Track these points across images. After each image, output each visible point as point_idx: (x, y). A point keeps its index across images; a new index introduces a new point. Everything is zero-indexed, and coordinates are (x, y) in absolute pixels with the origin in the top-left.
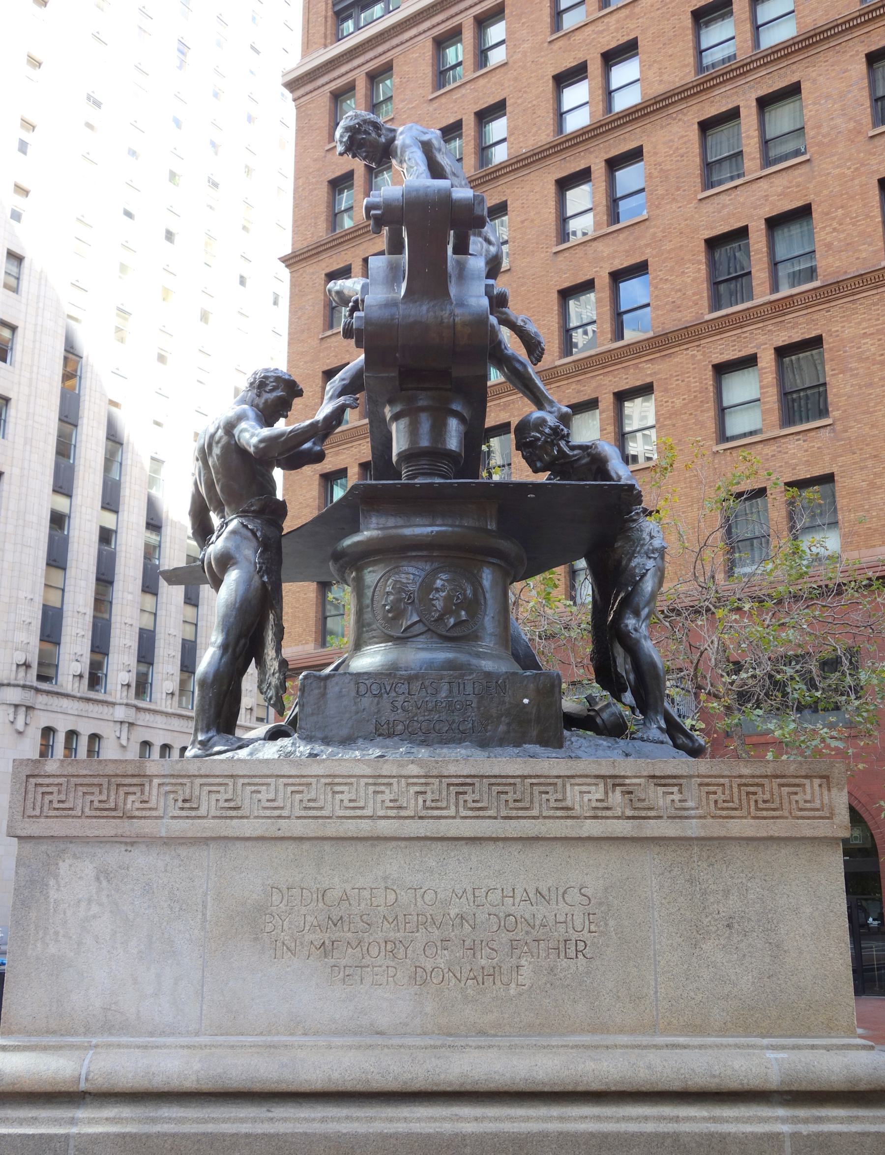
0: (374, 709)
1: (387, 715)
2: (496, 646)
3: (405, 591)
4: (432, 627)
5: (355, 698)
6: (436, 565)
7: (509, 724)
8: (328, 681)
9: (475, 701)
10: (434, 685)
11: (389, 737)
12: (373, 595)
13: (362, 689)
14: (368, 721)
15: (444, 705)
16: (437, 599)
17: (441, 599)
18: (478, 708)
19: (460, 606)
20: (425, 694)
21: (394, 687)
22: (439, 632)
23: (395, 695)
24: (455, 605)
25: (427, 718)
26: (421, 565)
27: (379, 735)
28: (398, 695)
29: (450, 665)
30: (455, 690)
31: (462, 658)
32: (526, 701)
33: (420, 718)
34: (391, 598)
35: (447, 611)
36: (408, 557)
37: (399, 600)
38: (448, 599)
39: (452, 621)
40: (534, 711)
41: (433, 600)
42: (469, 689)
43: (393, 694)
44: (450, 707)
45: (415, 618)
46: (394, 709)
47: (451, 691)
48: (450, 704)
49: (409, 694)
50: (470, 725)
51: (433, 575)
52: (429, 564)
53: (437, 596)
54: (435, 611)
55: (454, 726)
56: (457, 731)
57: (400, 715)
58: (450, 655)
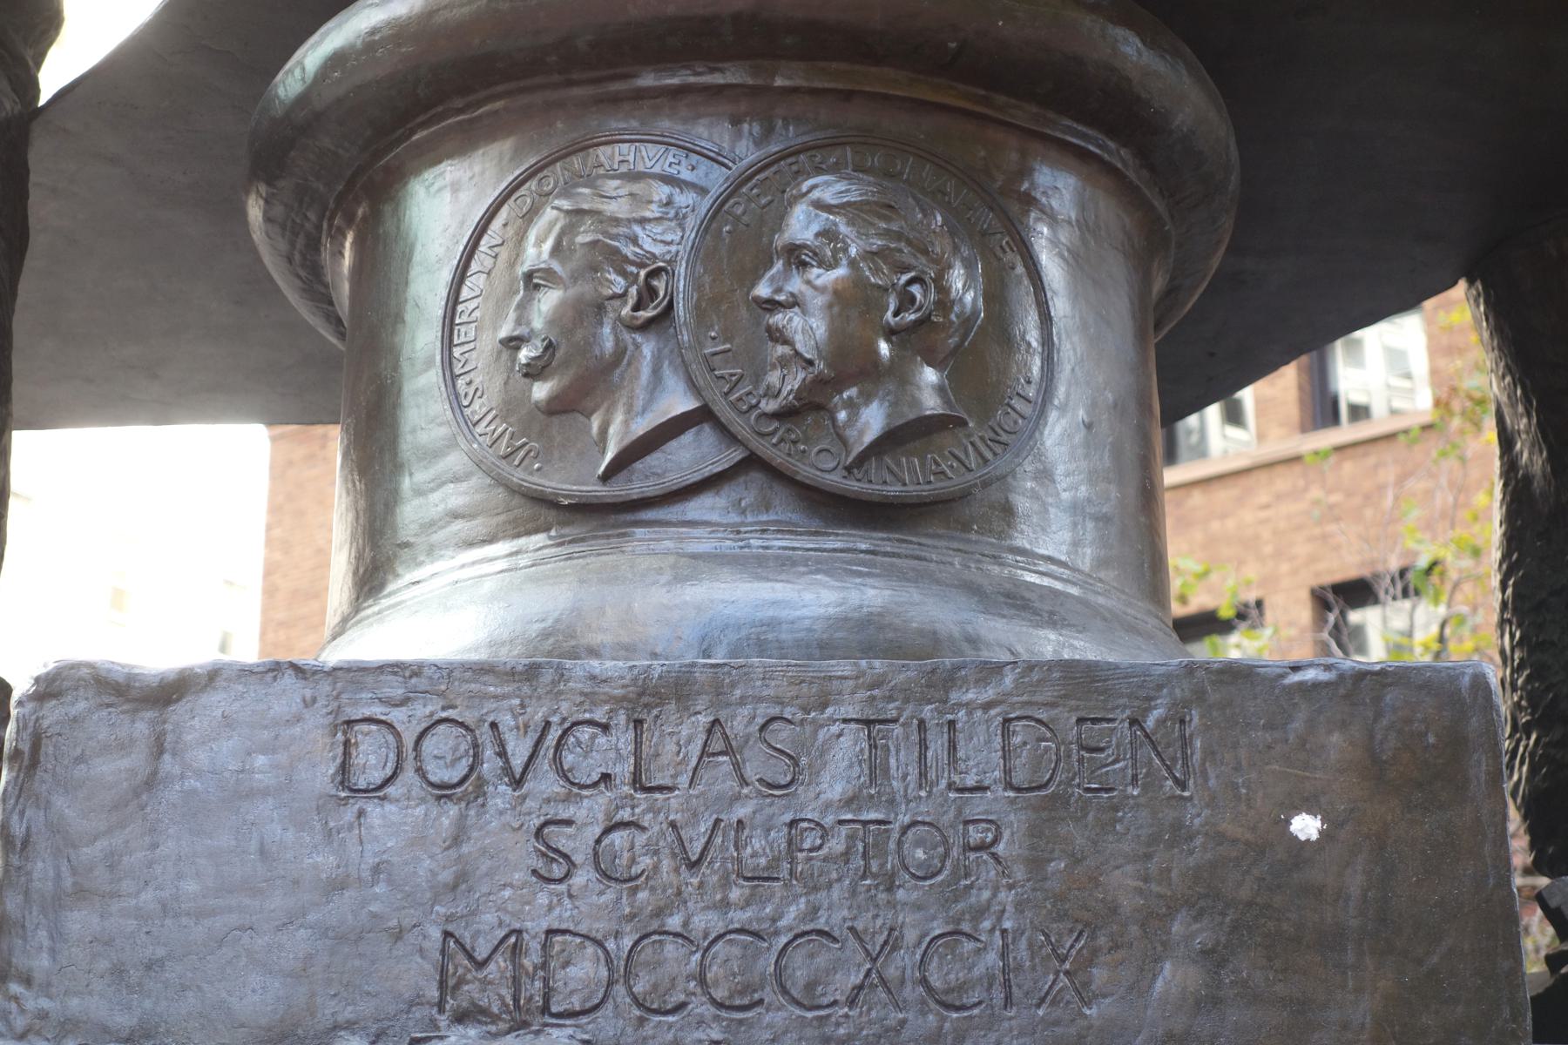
0: (429, 867)
1: (512, 900)
2: (1108, 575)
3: (618, 261)
4: (765, 449)
5: (328, 803)
6: (788, 136)
7: (1213, 958)
8: (178, 711)
9: (1015, 823)
10: (782, 736)
11: (520, 1026)
12: (454, 299)
13: (372, 759)
14: (398, 935)
15: (836, 845)
16: (795, 302)
17: (817, 301)
18: (1036, 864)
19: (918, 338)
20: (732, 784)
21: (553, 741)
22: (805, 472)
23: (556, 787)
24: (890, 333)
25: (739, 917)
26: (711, 133)
27: (461, 1018)
28: (575, 787)
29: (868, 637)
30: (901, 761)
31: (933, 611)
32: (1306, 826)
33: (700, 922)
34: (549, 301)
35: (847, 368)
36: (640, 95)
37: (589, 311)
38: (854, 302)
39: (873, 420)
40: (1355, 883)
41: (771, 305)
42: (981, 756)
43: (545, 783)
44: (873, 855)
45: (679, 402)
46: (552, 865)
47: (877, 770)
48: (871, 841)
49: (637, 782)
50: (992, 958)
51: (770, 185)
52: (752, 128)
53: (796, 285)
54: (783, 362)
55: (902, 962)
56: (912, 993)
57: (588, 902)
58: (872, 595)
